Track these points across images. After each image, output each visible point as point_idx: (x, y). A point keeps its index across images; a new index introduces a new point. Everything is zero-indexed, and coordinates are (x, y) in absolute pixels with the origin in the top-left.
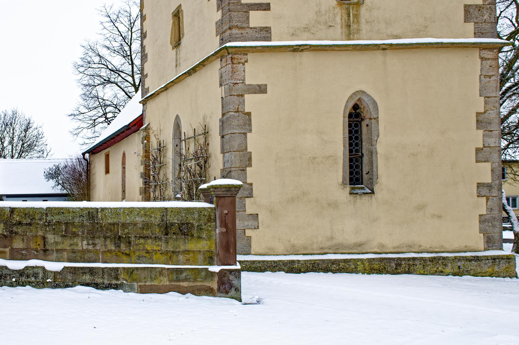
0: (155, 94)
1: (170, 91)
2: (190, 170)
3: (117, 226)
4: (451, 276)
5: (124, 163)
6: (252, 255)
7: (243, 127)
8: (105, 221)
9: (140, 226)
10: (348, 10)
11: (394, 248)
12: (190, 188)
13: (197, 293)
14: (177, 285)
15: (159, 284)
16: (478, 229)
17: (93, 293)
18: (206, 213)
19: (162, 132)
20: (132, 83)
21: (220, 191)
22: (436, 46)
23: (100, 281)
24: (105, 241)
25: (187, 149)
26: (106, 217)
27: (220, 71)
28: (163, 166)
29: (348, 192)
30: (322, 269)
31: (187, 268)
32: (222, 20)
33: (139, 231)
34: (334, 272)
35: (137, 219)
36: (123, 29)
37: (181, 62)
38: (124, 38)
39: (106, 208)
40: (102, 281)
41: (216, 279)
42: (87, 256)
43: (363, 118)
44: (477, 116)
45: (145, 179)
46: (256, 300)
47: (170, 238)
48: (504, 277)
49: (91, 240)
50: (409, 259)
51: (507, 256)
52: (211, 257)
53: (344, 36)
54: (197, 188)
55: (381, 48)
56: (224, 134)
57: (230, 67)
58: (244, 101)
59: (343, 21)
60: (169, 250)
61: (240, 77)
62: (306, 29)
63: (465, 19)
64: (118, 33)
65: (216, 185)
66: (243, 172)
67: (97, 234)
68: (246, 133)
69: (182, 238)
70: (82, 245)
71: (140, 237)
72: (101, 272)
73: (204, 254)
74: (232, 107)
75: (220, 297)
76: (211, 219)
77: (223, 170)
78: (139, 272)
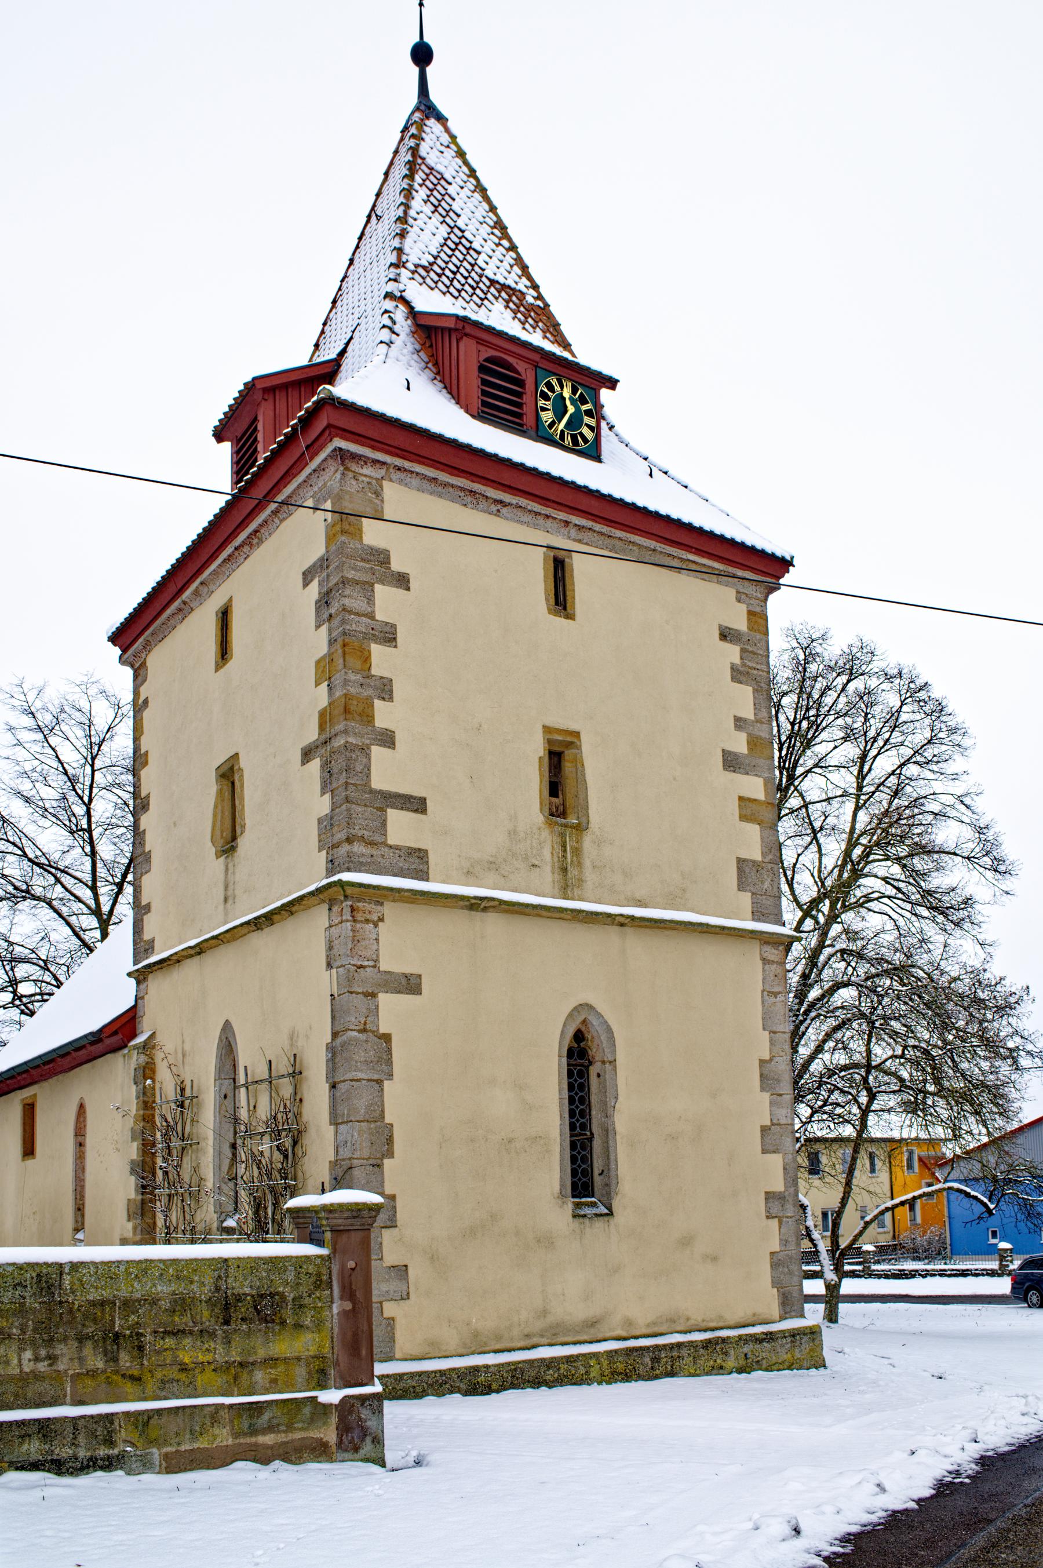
0: (170, 960)
1: (209, 959)
2: (260, 1161)
3: (111, 1308)
4: (735, 1375)
5: (80, 1131)
6: (397, 1360)
7: (376, 1066)
8: (81, 1295)
9: (165, 1304)
10: (562, 835)
11: (648, 1325)
12: (258, 1207)
13: (293, 1458)
14: (250, 1445)
15: (210, 1446)
16: (770, 1281)
17: (51, 1485)
18: (311, 1269)
19: (188, 1059)
20: (93, 906)
21: (340, 1218)
22: (700, 929)
23: (66, 1452)
24: (80, 1349)
25: (252, 1108)
26: (83, 1285)
27: (328, 933)
28: (191, 1145)
29: (570, 1212)
30: (529, 1381)
31: (272, 1401)
32: (332, 818)
33: (165, 1318)
34: (550, 1385)
35: (159, 1288)
36: (72, 757)
37: (237, 892)
38: (72, 780)
39: (82, 1263)
40: (71, 1452)
41: (334, 1420)
42: (33, 1390)
43: (591, 1060)
44: (760, 1067)
45: (143, 1178)
46: (413, 1459)
47: (235, 1330)
48: (808, 1369)
49: (45, 1347)
50: (672, 1347)
51: (810, 1328)
52: (323, 1370)
53: (556, 890)
54: (276, 1205)
55: (616, 922)
56: (337, 1080)
57: (350, 928)
58: (377, 1007)
59: (556, 860)
60: (232, 1359)
61: (368, 953)
62: (492, 865)
63: (739, 885)
64: (55, 764)
65: (332, 1205)
66: (376, 1169)
67: (61, 1330)
68: (382, 1081)
69: (260, 1330)
70: (20, 1362)
71: (165, 1332)
72: (69, 1429)
73: (308, 1364)
74: (353, 1019)
75: (343, 1461)
76: (321, 1281)
77: (333, 1164)
78: (164, 1419)
